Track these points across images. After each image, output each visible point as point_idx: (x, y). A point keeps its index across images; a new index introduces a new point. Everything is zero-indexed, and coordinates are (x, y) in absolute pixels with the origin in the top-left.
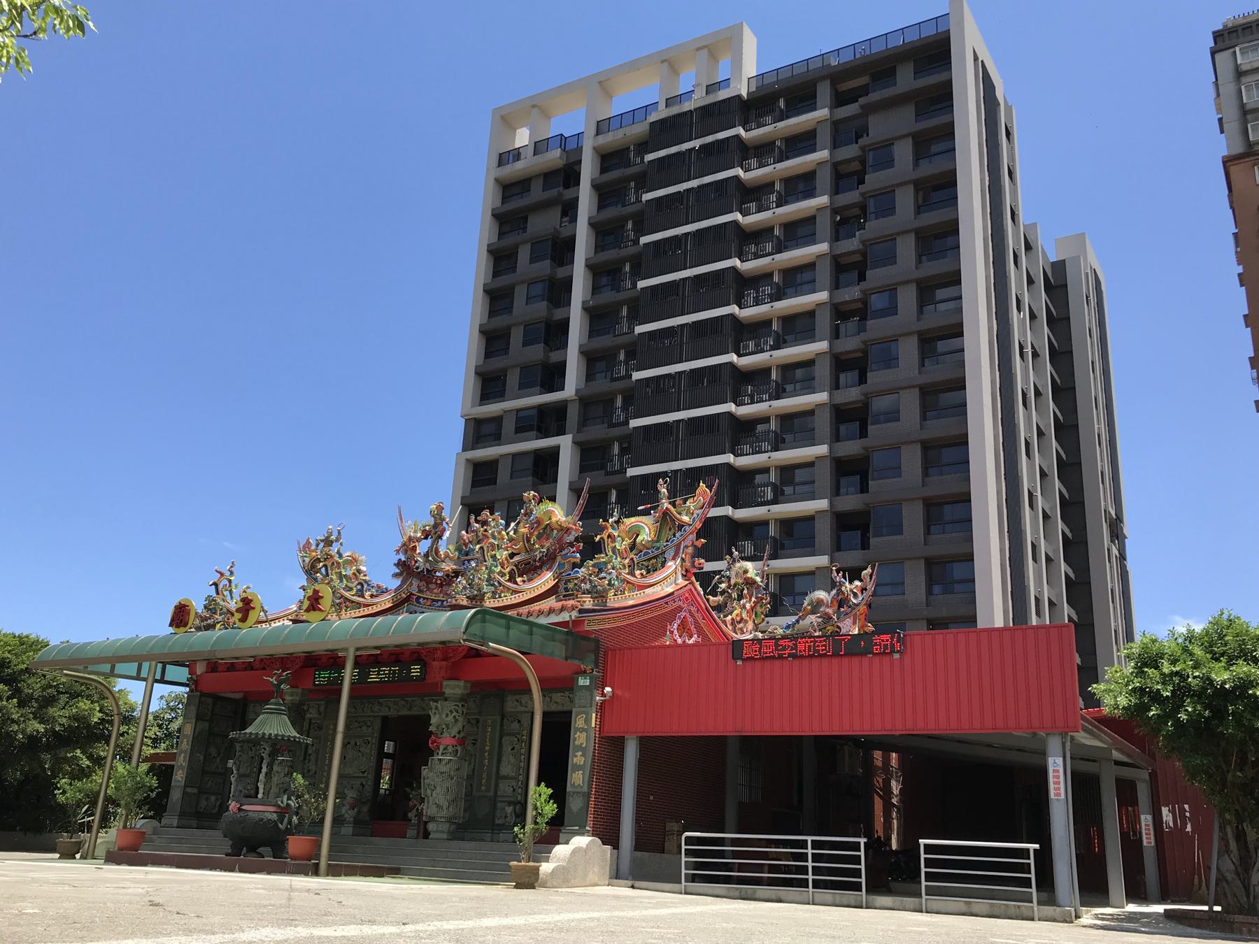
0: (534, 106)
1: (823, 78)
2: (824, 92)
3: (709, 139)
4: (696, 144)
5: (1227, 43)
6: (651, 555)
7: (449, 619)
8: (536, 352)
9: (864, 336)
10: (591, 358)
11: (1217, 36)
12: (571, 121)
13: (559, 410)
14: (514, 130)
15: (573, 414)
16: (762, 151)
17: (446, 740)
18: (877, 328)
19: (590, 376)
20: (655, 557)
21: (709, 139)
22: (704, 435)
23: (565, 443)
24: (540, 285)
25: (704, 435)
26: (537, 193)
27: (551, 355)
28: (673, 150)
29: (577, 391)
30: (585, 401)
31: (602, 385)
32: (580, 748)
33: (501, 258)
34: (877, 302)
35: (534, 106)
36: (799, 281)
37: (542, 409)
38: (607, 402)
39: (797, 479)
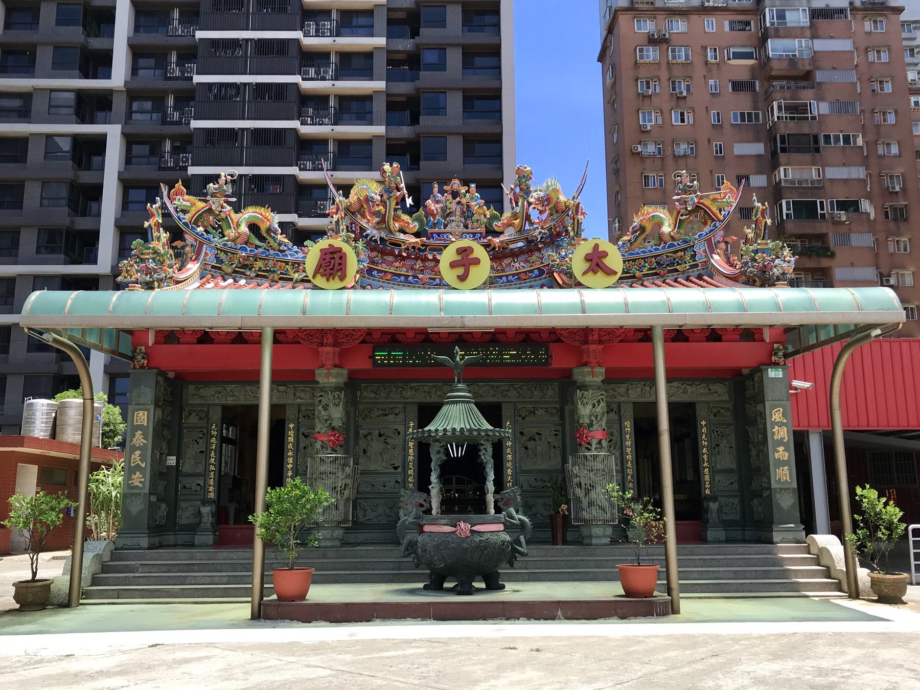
6: (678, 248)
7: (75, 301)
10: (137, 52)
15: (119, 105)
17: (597, 433)
18: (427, 78)
19: (134, 70)
20: (684, 250)
22: (268, 145)
23: (114, 134)
25: (268, 145)
27: (91, 40)
29: (126, 82)
30: (133, 94)
31: (149, 78)
32: (780, 442)
34: (429, 57)
36: (354, 23)
37: (81, 95)
38: (158, 99)
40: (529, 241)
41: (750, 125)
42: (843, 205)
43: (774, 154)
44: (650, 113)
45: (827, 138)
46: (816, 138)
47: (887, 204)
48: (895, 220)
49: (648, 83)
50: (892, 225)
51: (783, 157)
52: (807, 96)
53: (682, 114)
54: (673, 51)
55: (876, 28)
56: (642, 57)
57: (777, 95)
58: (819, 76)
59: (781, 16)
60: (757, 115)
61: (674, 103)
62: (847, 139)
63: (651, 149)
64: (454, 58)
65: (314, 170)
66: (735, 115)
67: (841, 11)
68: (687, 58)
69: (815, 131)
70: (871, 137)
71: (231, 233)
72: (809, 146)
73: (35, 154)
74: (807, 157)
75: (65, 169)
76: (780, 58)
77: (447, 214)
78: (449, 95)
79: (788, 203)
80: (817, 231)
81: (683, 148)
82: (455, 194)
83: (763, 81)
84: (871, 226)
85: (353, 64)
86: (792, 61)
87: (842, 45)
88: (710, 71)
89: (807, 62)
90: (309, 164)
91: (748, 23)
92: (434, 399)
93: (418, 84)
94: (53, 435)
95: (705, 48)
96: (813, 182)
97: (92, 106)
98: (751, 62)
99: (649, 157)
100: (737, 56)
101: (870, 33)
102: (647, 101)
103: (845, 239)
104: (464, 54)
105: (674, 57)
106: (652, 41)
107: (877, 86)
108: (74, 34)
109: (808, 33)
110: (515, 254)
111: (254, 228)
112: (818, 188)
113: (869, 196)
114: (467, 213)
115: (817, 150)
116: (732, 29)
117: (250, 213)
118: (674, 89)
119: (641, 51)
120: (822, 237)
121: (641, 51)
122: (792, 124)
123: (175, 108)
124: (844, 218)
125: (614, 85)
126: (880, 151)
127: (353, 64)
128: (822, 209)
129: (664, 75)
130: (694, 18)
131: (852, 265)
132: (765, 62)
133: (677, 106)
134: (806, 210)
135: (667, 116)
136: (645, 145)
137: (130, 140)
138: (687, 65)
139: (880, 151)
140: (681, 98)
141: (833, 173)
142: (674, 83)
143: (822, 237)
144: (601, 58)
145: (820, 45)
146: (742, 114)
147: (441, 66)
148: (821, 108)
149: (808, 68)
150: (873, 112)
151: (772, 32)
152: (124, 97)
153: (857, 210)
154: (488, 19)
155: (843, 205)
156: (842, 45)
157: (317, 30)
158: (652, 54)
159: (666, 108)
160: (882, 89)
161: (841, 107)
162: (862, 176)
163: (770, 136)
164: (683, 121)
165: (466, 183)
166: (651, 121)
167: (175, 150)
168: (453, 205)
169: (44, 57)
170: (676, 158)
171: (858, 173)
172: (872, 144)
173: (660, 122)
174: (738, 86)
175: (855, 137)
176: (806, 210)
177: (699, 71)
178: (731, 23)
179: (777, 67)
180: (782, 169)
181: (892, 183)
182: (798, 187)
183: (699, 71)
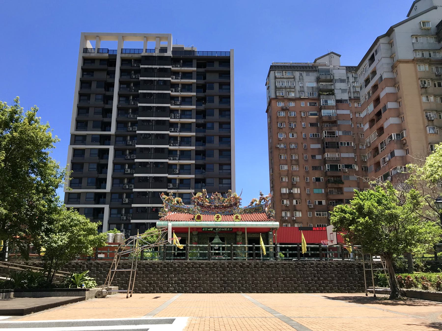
0: (97, 36)
1: (195, 59)
2: (195, 62)
3: (162, 67)
4: (158, 67)
5: (274, 69)
8: (99, 117)
9: (205, 134)
11: (271, 67)
12: (111, 44)
13: (109, 137)
14: (87, 40)
15: (113, 139)
16: (176, 74)
21: (162, 67)
23: (111, 148)
24: (101, 96)
26: (97, 65)
27: (104, 119)
28: (150, 66)
30: (116, 135)
31: (122, 132)
33: (84, 84)
34: (209, 125)
35: (97, 36)
38: (125, 137)
39: (185, 169)
40: (231, 205)
41: (316, 139)
42: (347, 166)
43: (324, 148)
44: (282, 134)
45: (341, 143)
46: (338, 143)
47: (363, 166)
48: (365, 171)
49: (281, 124)
50: (364, 173)
51: (326, 150)
52: (335, 129)
53: (293, 134)
54: (290, 113)
55: (359, 105)
56: (279, 115)
57: (325, 129)
58: (339, 122)
59: (326, 101)
60: (318, 135)
61: (290, 131)
62: (348, 144)
63: (282, 146)
64: (216, 126)
65: (173, 160)
66: (311, 134)
67: (346, 100)
68: (295, 115)
69: (337, 141)
70: (357, 142)
71: (173, 203)
72: (335, 146)
73: (87, 155)
74: (334, 150)
75: (96, 159)
76: (326, 116)
77: (215, 199)
78: (215, 137)
79: (328, 165)
80: (338, 175)
81: (293, 146)
82: (217, 195)
83: (320, 123)
84: (357, 173)
85: (185, 127)
86: (330, 117)
87: (347, 112)
88: (302, 119)
89: (335, 118)
90: (172, 158)
91: (316, 103)
92: (213, 236)
93: (205, 134)
94: (114, 242)
95: (301, 112)
96: (337, 158)
97: (105, 140)
98: (317, 117)
99: (281, 149)
100: (312, 115)
101: (356, 107)
102: (281, 130)
103: (347, 178)
104: (219, 137)
105: (290, 115)
106: (283, 109)
107: (359, 125)
108: (99, 117)
109: (335, 108)
110: (228, 207)
111: (178, 202)
112: (338, 160)
113: (356, 163)
114: (219, 199)
115: (338, 147)
116: (310, 105)
117: (177, 198)
118: (290, 126)
119: (279, 113)
120: (340, 177)
121: (279, 113)
122: (329, 138)
123: (130, 140)
124: (347, 171)
125: (270, 123)
126: (360, 147)
127: (185, 127)
128: (340, 167)
129: (287, 121)
130: (297, 101)
131: (350, 186)
132: (321, 117)
133: (291, 132)
134: (334, 168)
135: (287, 135)
136: (280, 145)
137: (116, 150)
138: (295, 117)
139: (360, 147)
140: (292, 129)
141: (344, 155)
142: (290, 124)
143: (340, 177)
144: (267, 111)
145: (339, 112)
146: (313, 134)
147: (212, 128)
148: (339, 133)
149: (335, 120)
150: (358, 134)
151: (323, 107)
152: (115, 137)
153: (351, 168)
154: (227, 113)
155: (347, 166)
156: (347, 112)
157: (174, 116)
158: (283, 114)
159: (287, 133)
160: (361, 126)
161: (345, 133)
162: (353, 156)
163: (322, 142)
164: (293, 136)
165: (219, 193)
166: (282, 136)
167: (130, 153)
168: (216, 197)
169: (90, 124)
170: (291, 149)
171: (352, 155)
172: (357, 145)
173: (285, 137)
174: (312, 125)
175: (351, 143)
176: (334, 168)
177: (299, 119)
178: (310, 103)
179: (324, 119)
180: (326, 154)
181: (364, 158)
182: (332, 160)
183: (299, 119)
